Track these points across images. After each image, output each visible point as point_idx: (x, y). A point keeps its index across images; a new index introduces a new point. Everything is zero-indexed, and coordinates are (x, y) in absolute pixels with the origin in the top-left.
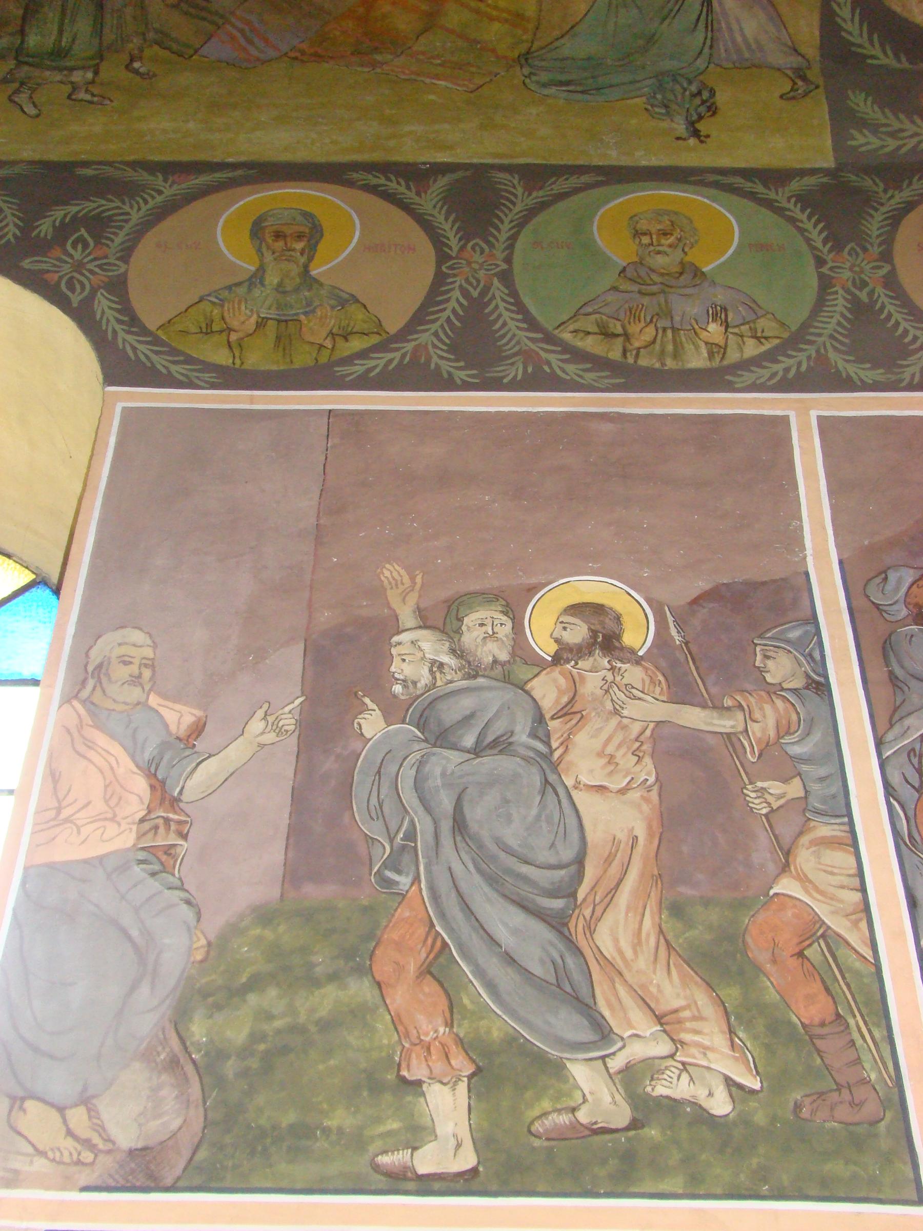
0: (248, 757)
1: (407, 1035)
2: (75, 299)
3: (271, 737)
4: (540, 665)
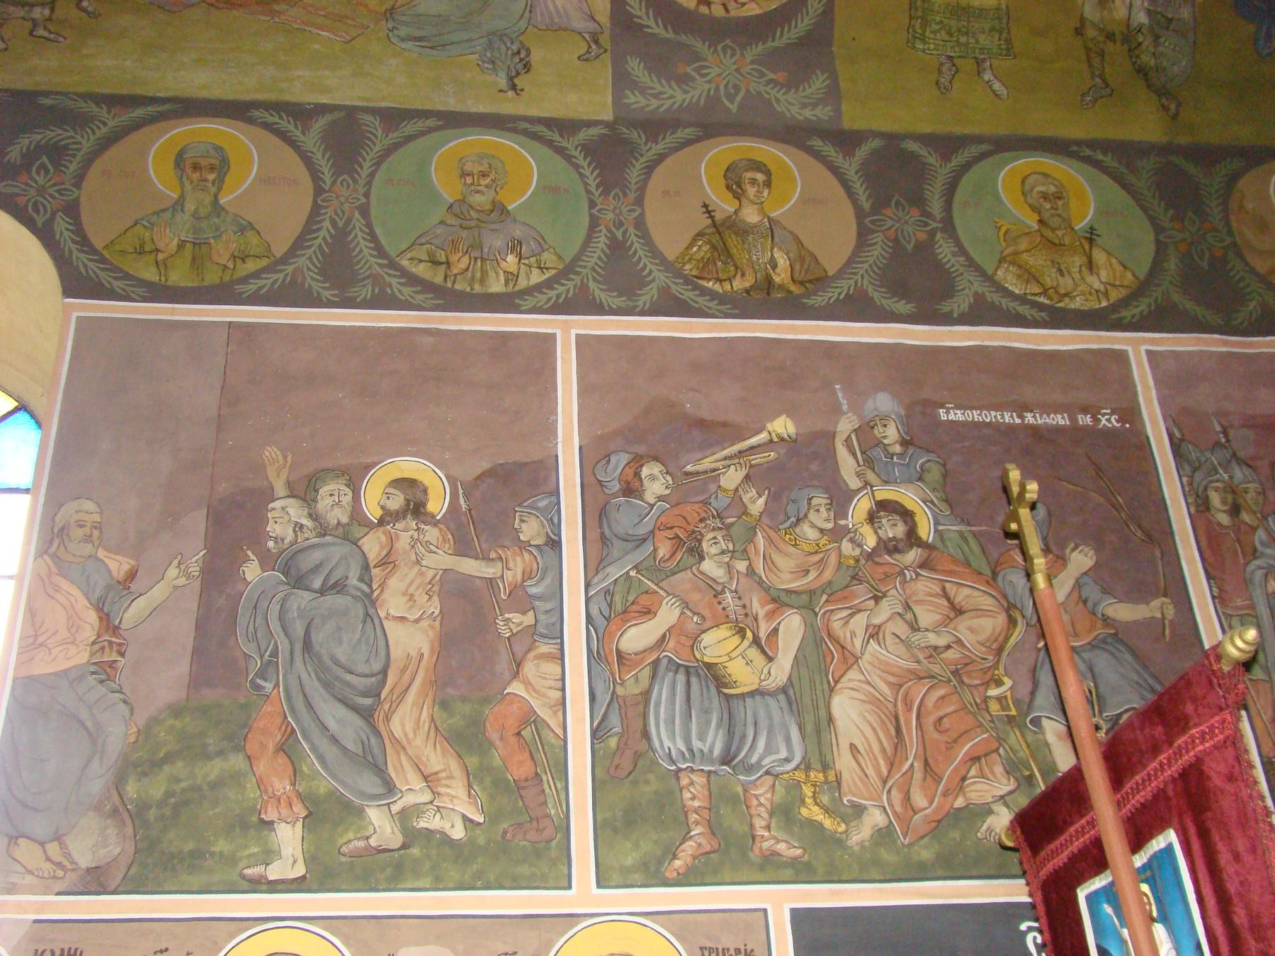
0: (170, 588)
1: (266, 792)
2: (40, 220)
3: (182, 581)
4: (370, 526)
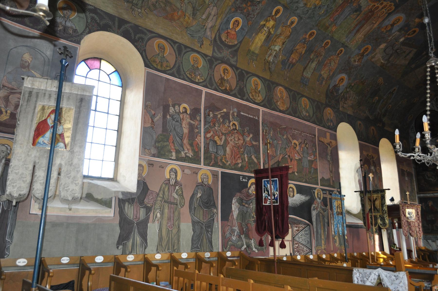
0: (159, 117)
